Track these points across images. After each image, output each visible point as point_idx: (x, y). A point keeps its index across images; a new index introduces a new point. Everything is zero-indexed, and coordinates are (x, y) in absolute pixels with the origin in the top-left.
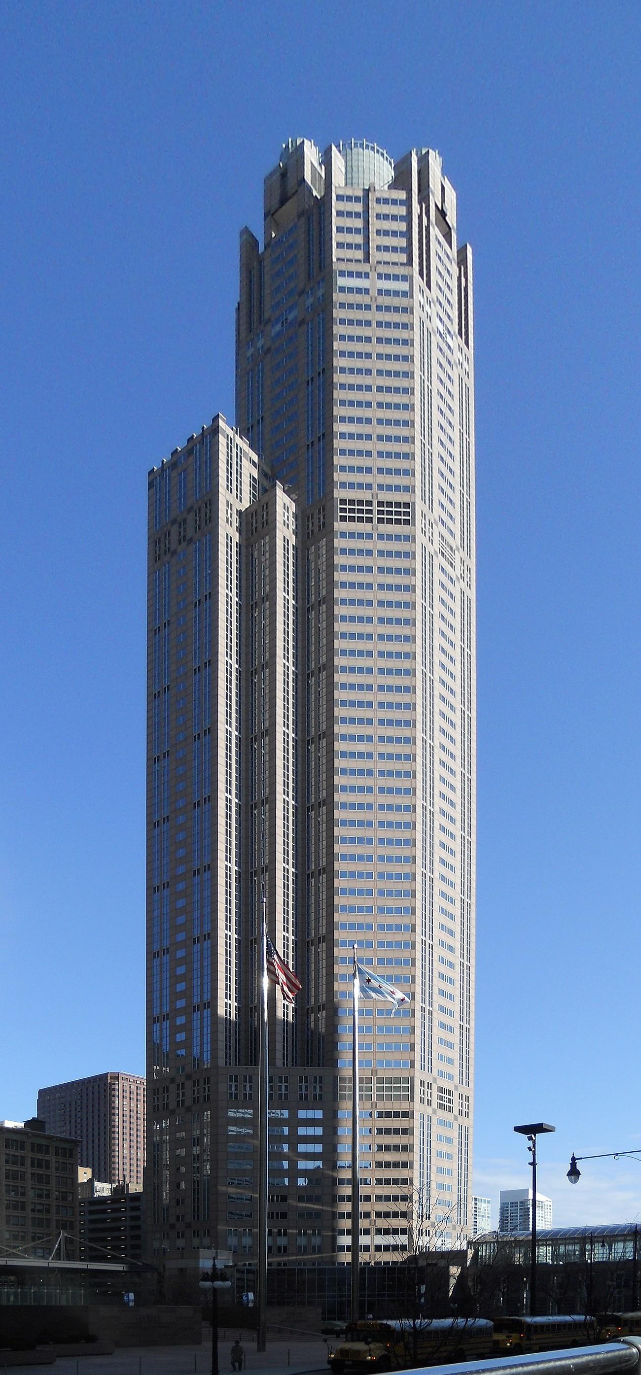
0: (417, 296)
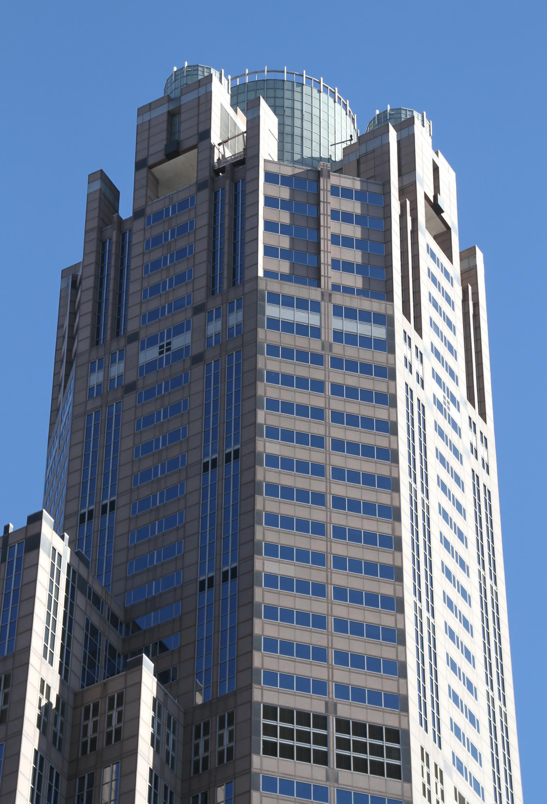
0: (401, 349)
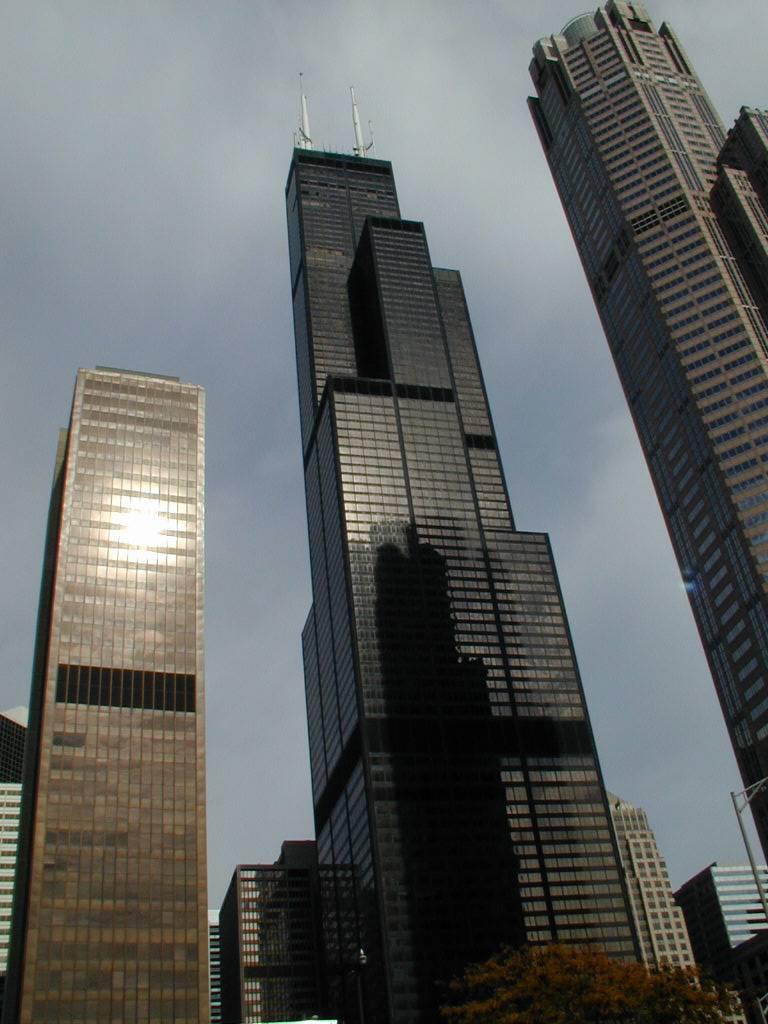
0: (634, 74)
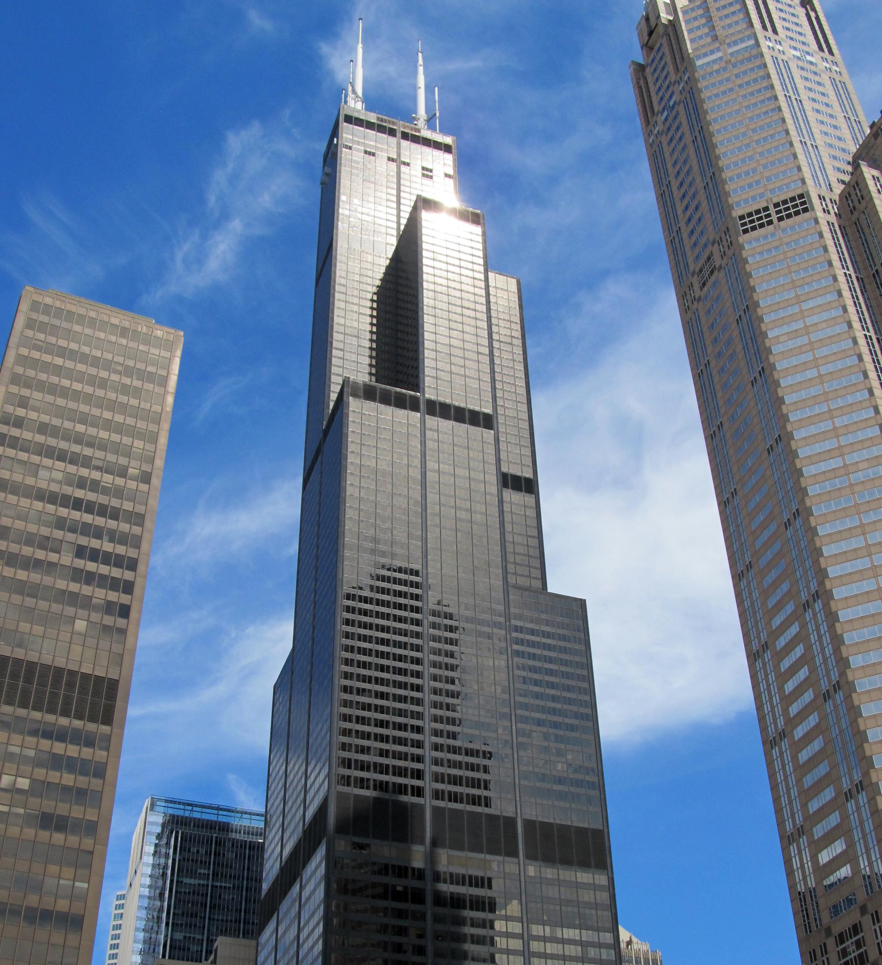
0: (764, 44)
